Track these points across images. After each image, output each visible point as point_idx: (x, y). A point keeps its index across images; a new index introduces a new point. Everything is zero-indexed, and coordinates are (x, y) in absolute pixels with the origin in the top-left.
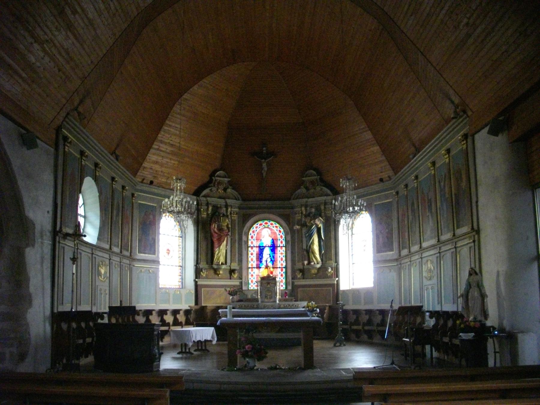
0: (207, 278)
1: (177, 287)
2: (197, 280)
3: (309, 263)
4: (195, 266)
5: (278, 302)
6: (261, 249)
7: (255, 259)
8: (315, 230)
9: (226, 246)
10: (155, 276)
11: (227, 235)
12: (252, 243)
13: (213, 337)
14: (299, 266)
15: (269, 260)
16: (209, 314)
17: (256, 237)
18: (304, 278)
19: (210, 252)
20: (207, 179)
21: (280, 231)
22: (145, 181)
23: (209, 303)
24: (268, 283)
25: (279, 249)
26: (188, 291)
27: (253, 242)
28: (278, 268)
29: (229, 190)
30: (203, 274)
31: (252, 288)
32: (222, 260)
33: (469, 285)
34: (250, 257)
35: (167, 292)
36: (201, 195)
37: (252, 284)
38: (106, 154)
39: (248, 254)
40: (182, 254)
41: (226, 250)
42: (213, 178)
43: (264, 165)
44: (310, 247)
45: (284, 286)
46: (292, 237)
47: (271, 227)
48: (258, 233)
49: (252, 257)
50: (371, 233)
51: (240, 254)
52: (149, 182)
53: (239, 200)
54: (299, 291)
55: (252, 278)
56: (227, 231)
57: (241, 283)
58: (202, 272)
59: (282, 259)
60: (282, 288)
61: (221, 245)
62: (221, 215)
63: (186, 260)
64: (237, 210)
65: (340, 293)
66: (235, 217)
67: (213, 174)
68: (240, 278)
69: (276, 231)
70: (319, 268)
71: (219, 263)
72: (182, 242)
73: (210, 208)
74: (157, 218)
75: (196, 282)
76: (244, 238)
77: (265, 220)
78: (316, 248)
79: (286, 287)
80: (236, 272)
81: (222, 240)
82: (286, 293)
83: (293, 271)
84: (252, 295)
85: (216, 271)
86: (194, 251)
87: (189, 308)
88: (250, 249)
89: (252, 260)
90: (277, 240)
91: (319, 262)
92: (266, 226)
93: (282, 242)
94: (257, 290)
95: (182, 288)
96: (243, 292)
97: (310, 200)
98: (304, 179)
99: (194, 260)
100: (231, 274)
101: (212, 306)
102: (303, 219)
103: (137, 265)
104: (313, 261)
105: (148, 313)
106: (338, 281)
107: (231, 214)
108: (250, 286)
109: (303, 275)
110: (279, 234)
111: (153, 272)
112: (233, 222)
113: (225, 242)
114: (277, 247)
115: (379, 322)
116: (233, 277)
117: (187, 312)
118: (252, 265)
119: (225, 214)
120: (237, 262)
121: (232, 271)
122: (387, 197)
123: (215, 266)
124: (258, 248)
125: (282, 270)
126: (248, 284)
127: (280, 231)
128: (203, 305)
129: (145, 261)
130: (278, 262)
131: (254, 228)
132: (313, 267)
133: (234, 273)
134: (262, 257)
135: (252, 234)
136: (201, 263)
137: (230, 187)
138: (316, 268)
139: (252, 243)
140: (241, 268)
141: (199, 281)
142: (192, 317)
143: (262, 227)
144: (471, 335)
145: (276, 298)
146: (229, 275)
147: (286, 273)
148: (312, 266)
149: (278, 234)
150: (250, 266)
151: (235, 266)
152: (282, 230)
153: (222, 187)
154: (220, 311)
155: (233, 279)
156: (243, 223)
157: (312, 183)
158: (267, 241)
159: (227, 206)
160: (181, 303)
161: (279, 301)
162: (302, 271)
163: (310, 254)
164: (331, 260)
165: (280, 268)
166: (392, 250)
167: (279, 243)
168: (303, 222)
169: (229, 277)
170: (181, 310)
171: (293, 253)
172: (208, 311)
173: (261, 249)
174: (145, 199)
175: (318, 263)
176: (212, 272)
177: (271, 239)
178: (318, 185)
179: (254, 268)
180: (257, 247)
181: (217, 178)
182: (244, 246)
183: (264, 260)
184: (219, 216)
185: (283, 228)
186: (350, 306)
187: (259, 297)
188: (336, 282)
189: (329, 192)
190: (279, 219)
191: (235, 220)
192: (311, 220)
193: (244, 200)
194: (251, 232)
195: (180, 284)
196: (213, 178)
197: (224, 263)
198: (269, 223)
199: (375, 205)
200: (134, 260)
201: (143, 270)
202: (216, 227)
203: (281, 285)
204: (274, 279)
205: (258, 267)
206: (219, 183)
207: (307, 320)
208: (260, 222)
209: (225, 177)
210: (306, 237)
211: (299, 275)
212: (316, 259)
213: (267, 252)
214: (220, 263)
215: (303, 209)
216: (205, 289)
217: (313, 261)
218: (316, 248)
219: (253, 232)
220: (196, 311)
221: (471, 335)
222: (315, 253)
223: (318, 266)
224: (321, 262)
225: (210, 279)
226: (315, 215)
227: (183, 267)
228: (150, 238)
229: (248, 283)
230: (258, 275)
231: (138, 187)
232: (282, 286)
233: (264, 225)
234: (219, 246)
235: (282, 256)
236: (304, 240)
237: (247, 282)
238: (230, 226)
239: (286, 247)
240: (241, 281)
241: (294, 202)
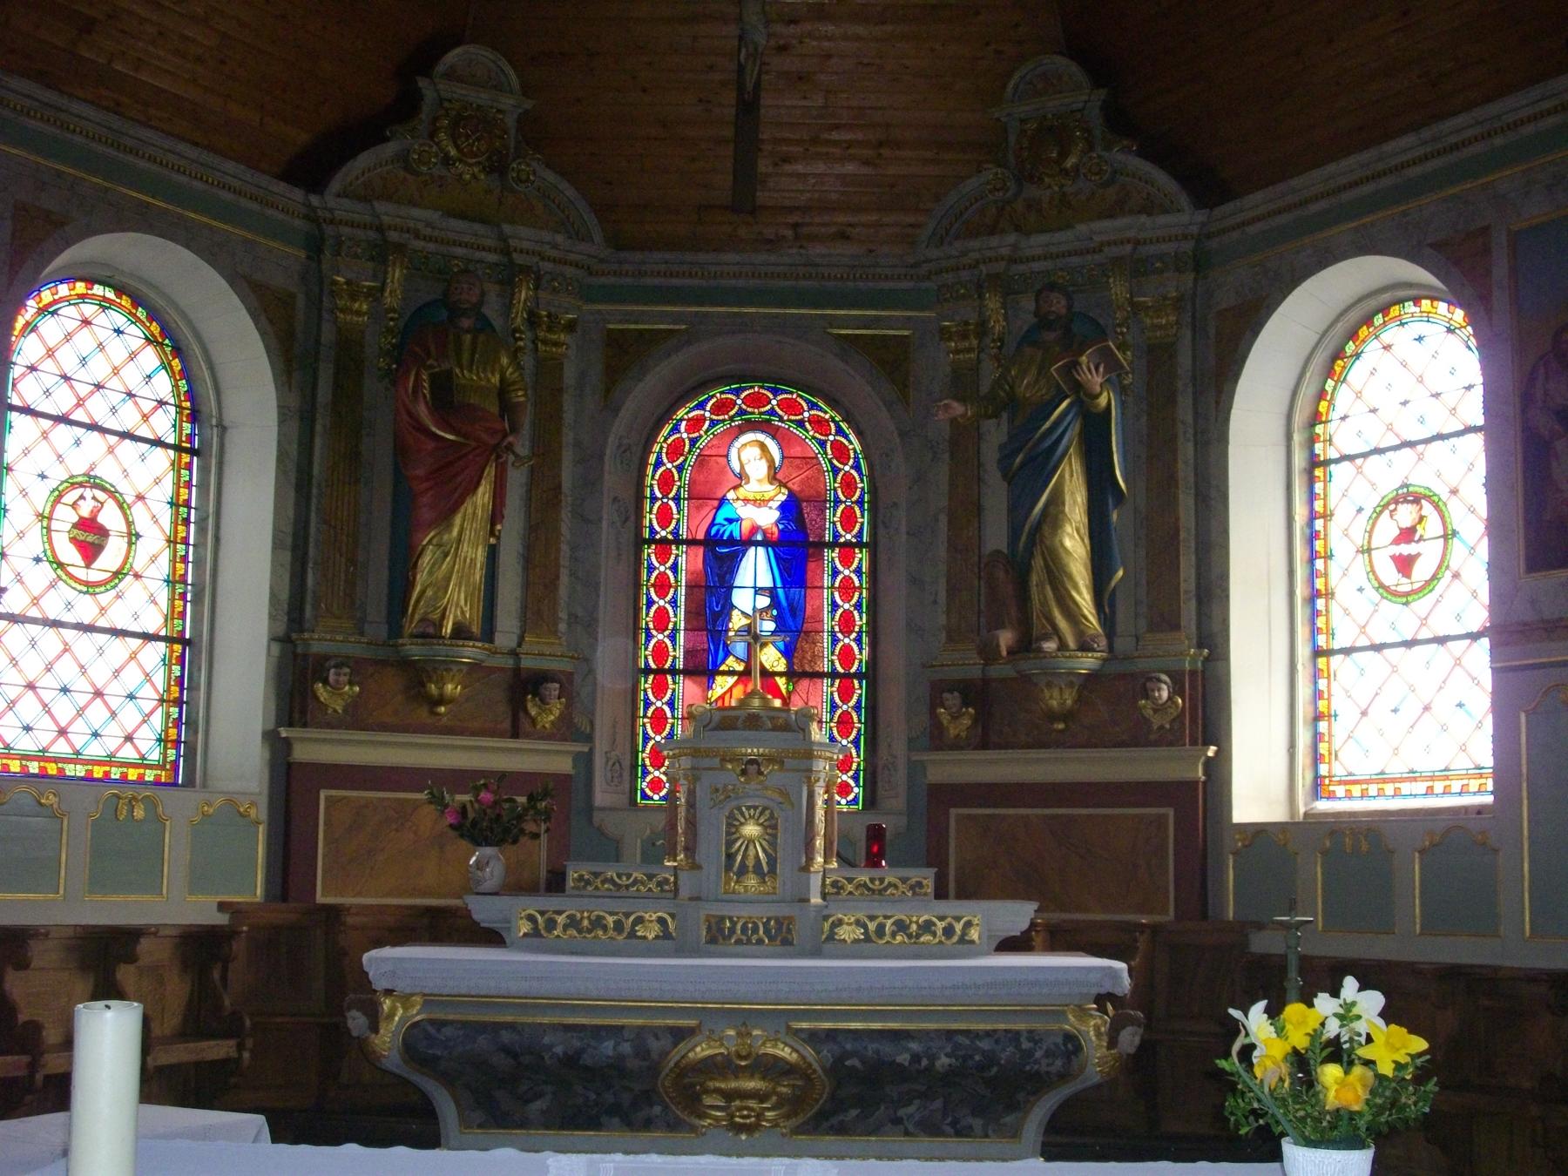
0: (356, 719)
3: (1027, 644)
4: (274, 639)
5: (816, 900)
8: (1072, 436)
9: (496, 516)
12: (665, 517)
14: (969, 665)
17: (692, 482)
18: (984, 745)
21: (841, 452)
26: (219, 801)
28: (821, 675)
30: (331, 696)
32: (460, 605)
36: (335, 185)
41: (492, 554)
42: (422, 83)
47: (785, 422)
48: (702, 460)
54: (1162, 810)
58: (326, 682)
59: (847, 623)
61: (454, 510)
63: (219, 600)
69: (816, 448)
70: (1093, 677)
71: (440, 625)
72: (203, 487)
77: (755, 379)
78: (1074, 544)
79: (871, 801)
86: (277, 545)
87: (222, 919)
88: (649, 552)
89: (662, 619)
90: (820, 502)
91: (1094, 638)
92: (755, 414)
93: (848, 520)
95: (190, 782)
96: (597, 817)
99: (274, 597)
100: (517, 707)
101: (382, 909)
109: (984, 719)
110: (836, 471)
113: (483, 495)
114: (822, 545)
115: (1315, 1000)
116: (533, 721)
118: (660, 652)
125: (846, 694)
127: (841, 452)
139: (665, 517)
141: (303, 740)
146: (503, 710)
147: (872, 709)
149: (825, 466)
155: (528, 736)
160: (150, 881)
161: (824, 896)
162: (976, 694)
164: (1176, 627)
165: (833, 675)
169: (507, 725)
175: (1085, 647)
179: (673, 671)
180: (691, 542)
194: (660, 446)
196: (422, 83)
197: (475, 629)
208: (717, 394)
210: (1008, 476)
211: (960, 725)
213: (756, 569)
214: (448, 628)
216: (333, 792)
217: (1056, 630)
218: (1074, 544)
219: (675, 450)
222: (1070, 577)
223: (1087, 663)
224: (1103, 642)
225: (384, 727)
229: (634, 766)
232: (844, 789)
233: (741, 412)
237: (627, 763)
239: (873, 547)
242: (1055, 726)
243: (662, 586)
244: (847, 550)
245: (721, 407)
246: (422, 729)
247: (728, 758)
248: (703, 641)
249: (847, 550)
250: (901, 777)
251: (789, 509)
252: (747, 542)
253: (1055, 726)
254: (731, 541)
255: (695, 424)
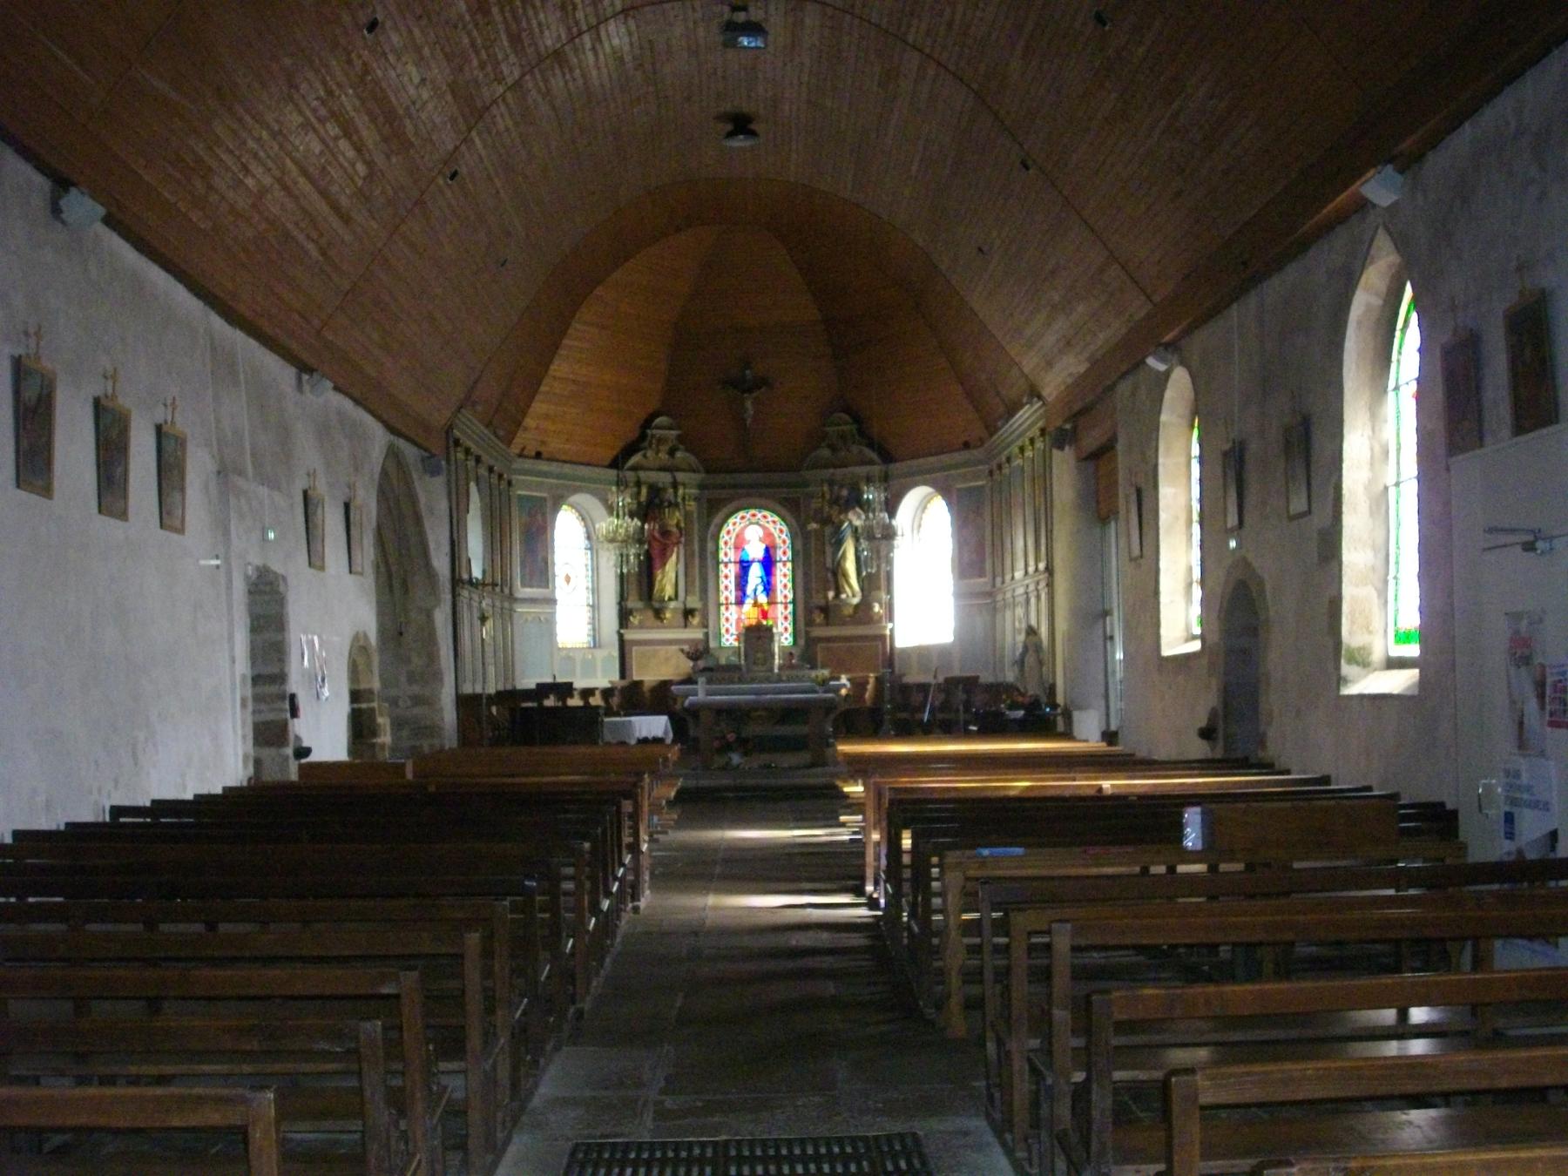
0: (641, 626)
1: (585, 646)
2: (622, 631)
6: (744, 566)
7: (732, 587)
10: (549, 624)
11: (678, 543)
12: (726, 554)
13: (666, 732)
14: (818, 600)
15: (761, 588)
16: (647, 695)
19: (645, 580)
20: (633, 435)
22: (526, 453)
23: (649, 673)
24: (759, 638)
25: (779, 565)
27: (727, 553)
29: (679, 455)
30: (634, 620)
31: (728, 644)
33: (1026, 648)
34: (723, 582)
35: (569, 655)
37: (727, 636)
38: (469, 420)
39: (717, 576)
40: (593, 581)
42: (649, 431)
43: (749, 404)
44: (839, 562)
45: (791, 639)
46: (805, 545)
47: (763, 522)
49: (726, 582)
50: (951, 540)
51: (704, 580)
52: (533, 454)
53: (699, 472)
55: (727, 625)
56: (678, 535)
57: (707, 635)
59: (785, 586)
60: (786, 643)
62: (666, 504)
64: (694, 491)
65: (896, 652)
66: (692, 506)
67: (647, 423)
68: (704, 625)
72: (592, 559)
73: (644, 491)
74: (548, 520)
75: (621, 636)
76: (710, 545)
80: (697, 613)
81: (668, 553)
82: (791, 654)
83: (809, 611)
84: (728, 658)
85: (658, 614)
87: (609, 685)
88: (722, 567)
89: (726, 588)
92: (754, 520)
93: (785, 553)
94: (739, 648)
95: (595, 646)
97: (839, 471)
98: (828, 429)
102: (827, 509)
103: (520, 609)
104: (845, 592)
105: (587, 693)
106: (892, 630)
107: (684, 499)
108: (723, 640)
109: (827, 617)
111: (547, 620)
112: (687, 516)
113: (674, 557)
117: (607, 693)
118: (727, 598)
119: (673, 500)
120: (698, 594)
121: (688, 613)
122: (976, 477)
123: (656, 605)
124: (738, 565)
125: (786, 608)
126: (719, 636)
127: (781, 531)
128: (636, 678)
129: (533, 601)
130: (779, 592)
131: (731, 525)
132: (845, 603)
133: (693, 616)
134: (747, 582)
135: (727, 538)
136: (631, 598)
137: (681, 447)
138: (850, 605)
139: (726, 554)
140: (705, 605)
142: (615, 701)
143: (746, 522)
144: (1021, 713)
145: (773, 663)
146: (682, 620)
148: (842, 600)
149: (776, 535)
150: (722, 600)
151: (694, 602)
152: (785, 528)
153: (665, 448)
154: (673, 688)
156: (708, 516)
157: (843, 437)
158: (755, 551)
159: (675, 485)
163: (840, 577)
166: (985, 576)
167: (779, 555)
168: (825, 515)
169: (683, 624)
170: (597, 689)
171: (806, 574)
172: (646, 687)
173: (744, 566)
174: (528, 486)
175: (854, 596)
176: (650, 614)
177: (764, 546)
178: (854, 443)
181: (654, 431)
182: (710, 562)
183: (749, 590)
184: (660, 506)
185: (787, 525)
186: (913, 678)
187: (743, 662)
188: (888, 632)
189: (874, 456)
190: (778, 507)
191: (692, 512)
192: (840, 513)
193: (707, 472)
194: (723, 533)
195: (590, 639)
197: (673, 597)
198: (759, 516)
199: (959, 490)
200: (516, 600)
201: (530, 618)
202: (657, 527)
203: (784, 637)
204: (769, 629)
205: (740, 602)
206: (661, 441)
207: (815, 699)
209: (670, 428)
212: (850, 586)
214: (666, 598)
215: (826, 488)
219: (728, 532)
220: (624, 690)
221: (1021, 713)
223: (856, 601)
226: (847, 501)
227: (595, 608)
228: (540, 558)
230: (739, 620)
231: (515, 466)
234: (664, 564)
235: (785, 581)
236: (828, 550)
238: (682, 525)
240: (705, 630)
241: (808, 474)
242: (495, 713)
243: (726, 577)
244: (785, 564)
245: (743, 518)
246: (658, 627)
247: (463, 148)
248: (740, 593)
249: (785, 564)
250: (803, 634)
251: (767, 550)
252: (753, 561)
253: (495, 713)
254: (748, 562)
255: (734, 524)
